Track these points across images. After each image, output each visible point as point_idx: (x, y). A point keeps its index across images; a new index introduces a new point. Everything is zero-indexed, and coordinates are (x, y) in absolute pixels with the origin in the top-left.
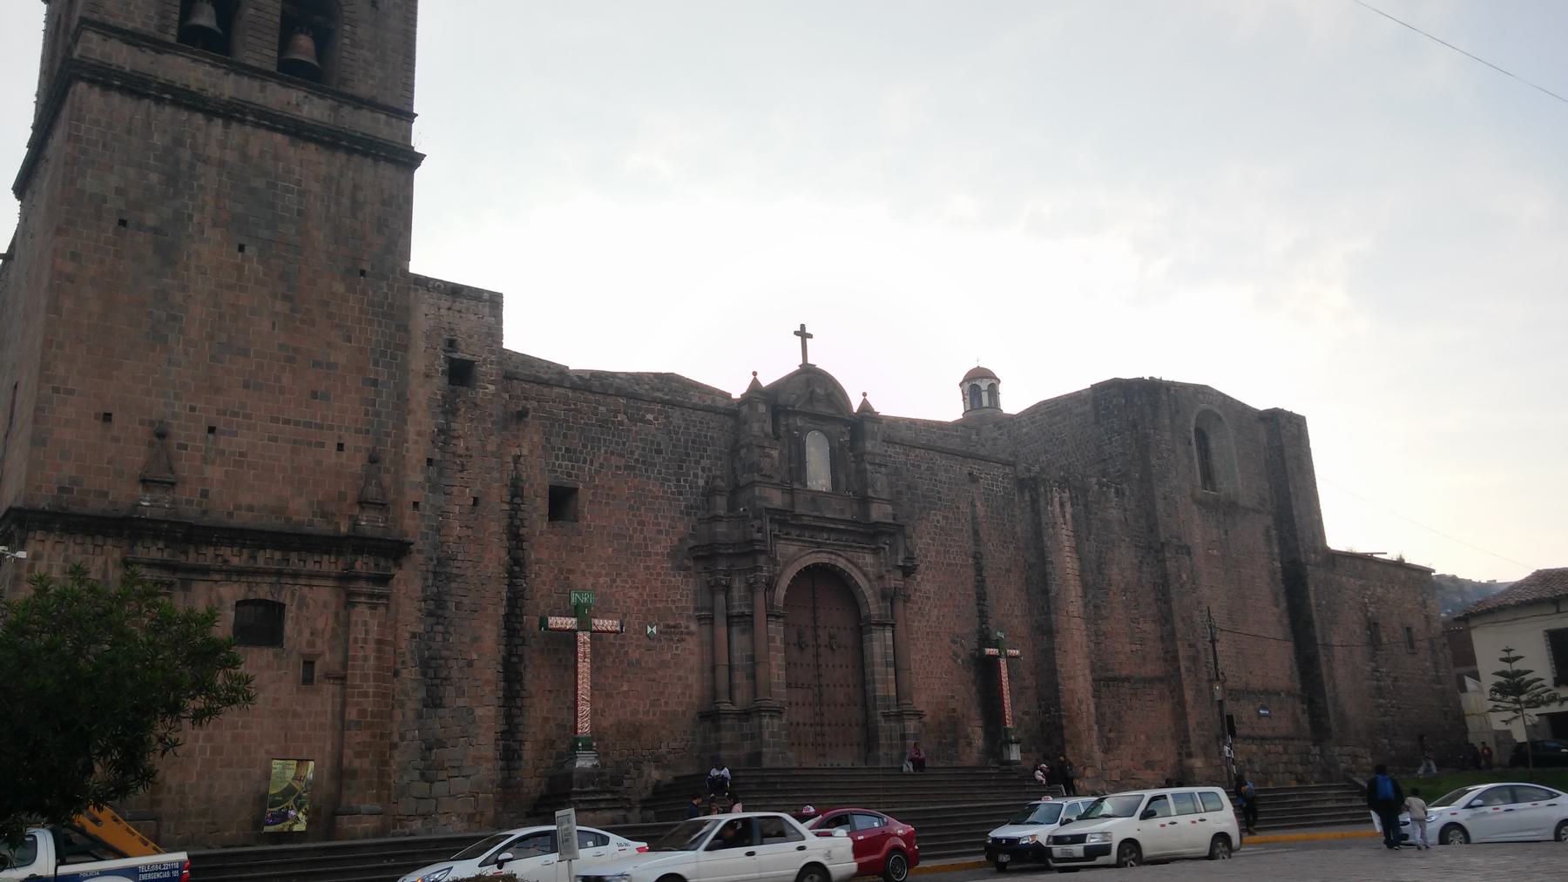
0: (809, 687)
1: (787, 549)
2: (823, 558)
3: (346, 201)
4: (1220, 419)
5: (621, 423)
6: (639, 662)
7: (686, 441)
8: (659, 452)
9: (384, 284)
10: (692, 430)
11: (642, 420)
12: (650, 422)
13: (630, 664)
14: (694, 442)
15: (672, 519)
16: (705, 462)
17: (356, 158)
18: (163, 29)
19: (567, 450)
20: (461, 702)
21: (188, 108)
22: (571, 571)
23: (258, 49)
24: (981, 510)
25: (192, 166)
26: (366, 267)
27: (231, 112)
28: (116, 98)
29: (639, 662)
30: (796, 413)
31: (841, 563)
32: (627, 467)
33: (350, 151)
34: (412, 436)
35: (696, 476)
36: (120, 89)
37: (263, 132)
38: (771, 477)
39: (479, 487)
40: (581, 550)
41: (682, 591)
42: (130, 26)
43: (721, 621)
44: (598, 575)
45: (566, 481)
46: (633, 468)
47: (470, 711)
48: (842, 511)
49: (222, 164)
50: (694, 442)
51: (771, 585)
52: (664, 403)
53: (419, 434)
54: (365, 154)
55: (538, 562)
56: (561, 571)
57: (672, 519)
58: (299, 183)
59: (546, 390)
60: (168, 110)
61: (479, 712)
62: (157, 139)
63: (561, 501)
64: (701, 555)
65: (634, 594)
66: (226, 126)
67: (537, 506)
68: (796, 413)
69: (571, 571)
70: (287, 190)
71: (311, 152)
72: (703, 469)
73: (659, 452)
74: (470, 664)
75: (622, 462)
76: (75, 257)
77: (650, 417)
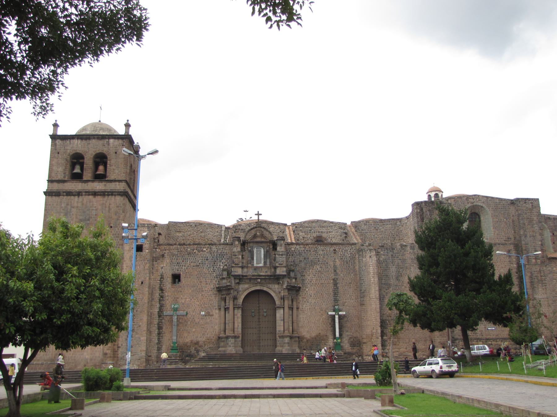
0: (255, 328)
1: (242, 287)
2: (258, 288)
3: (107, 209)
4: (482, 207)
5: (195, 253)
6: (199, 323)
7: (217, 255)
8: (207, 260)
9: (117, 229)
10: (219, 251)
11: (202, 251)
12: (205, 251)
13: (196, 323)
14: (220, 255)
15: (211, 280)
16: (223, 261)
17: (110, 196)
18: (64, 177)
19: (178, 263)
20: (137, 336)
21: (70, 195)
22: (177, 298)
23: (88, 175)
24: (338, 263)
25: (71, 210)
26: (112, 225)
27: (79, 194)
28: (54, 198)
29: (199, 323)
30: (250, 242)
31: (265, 289)
32: (197, 266)
33: (108, 195)
34: (125, 267)
35: (220, 265)
36: (55, 195)
37: (87, 196)
38: (238, 264)
39: (143, 279)
40: (181, 292)
41: (215, 300)
42: (57, 179)
43: (223, 309)
44: (186, 298)
45: (177, 272)
46: (198, 266)
47: (139, 338)
48: (266, 272)
49: (77, 207)
50: (220, 255)
51: (235, 298)
52: (209, 244)
53: (127, 267)
54: (112, 195)
55: (168, 296)
56: (175, 298)
57: (211, 280)
58: (95, 207)
59: (171, 247)
60: (65, 197)
61: (142, 338)
62: (63, 205)
63: (176, 278)
64: (219, 290)
65: (198, 303)
66: (78, 197)
67: (168, 280)
68: (250, 242)
69: (177, 298)
70: (92, 210)
71: (99, 198)
72: (223, 263)
73: (207, 260)
74: (140, 326)
75: (195, 264)
76: (82, 227)
77: (205, 249)
